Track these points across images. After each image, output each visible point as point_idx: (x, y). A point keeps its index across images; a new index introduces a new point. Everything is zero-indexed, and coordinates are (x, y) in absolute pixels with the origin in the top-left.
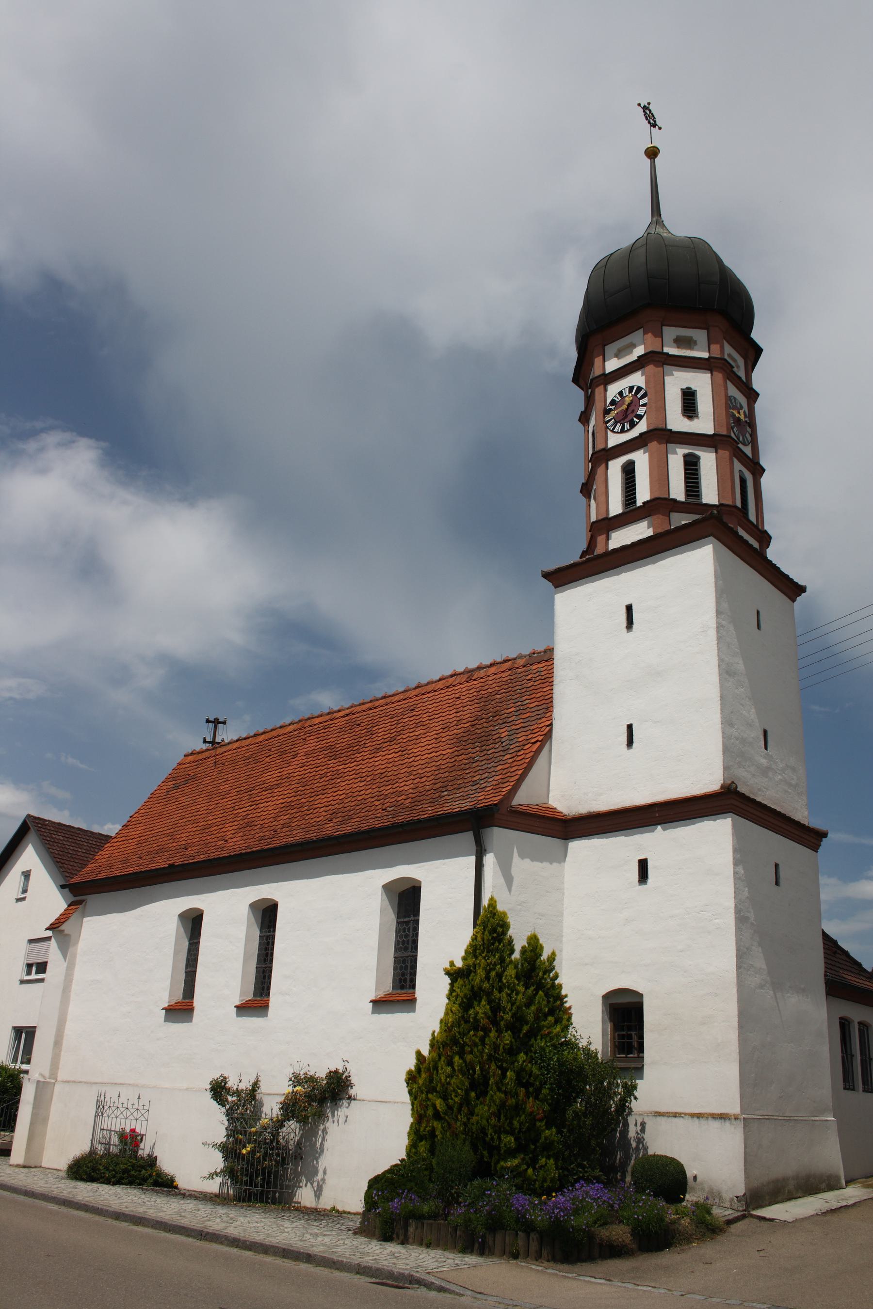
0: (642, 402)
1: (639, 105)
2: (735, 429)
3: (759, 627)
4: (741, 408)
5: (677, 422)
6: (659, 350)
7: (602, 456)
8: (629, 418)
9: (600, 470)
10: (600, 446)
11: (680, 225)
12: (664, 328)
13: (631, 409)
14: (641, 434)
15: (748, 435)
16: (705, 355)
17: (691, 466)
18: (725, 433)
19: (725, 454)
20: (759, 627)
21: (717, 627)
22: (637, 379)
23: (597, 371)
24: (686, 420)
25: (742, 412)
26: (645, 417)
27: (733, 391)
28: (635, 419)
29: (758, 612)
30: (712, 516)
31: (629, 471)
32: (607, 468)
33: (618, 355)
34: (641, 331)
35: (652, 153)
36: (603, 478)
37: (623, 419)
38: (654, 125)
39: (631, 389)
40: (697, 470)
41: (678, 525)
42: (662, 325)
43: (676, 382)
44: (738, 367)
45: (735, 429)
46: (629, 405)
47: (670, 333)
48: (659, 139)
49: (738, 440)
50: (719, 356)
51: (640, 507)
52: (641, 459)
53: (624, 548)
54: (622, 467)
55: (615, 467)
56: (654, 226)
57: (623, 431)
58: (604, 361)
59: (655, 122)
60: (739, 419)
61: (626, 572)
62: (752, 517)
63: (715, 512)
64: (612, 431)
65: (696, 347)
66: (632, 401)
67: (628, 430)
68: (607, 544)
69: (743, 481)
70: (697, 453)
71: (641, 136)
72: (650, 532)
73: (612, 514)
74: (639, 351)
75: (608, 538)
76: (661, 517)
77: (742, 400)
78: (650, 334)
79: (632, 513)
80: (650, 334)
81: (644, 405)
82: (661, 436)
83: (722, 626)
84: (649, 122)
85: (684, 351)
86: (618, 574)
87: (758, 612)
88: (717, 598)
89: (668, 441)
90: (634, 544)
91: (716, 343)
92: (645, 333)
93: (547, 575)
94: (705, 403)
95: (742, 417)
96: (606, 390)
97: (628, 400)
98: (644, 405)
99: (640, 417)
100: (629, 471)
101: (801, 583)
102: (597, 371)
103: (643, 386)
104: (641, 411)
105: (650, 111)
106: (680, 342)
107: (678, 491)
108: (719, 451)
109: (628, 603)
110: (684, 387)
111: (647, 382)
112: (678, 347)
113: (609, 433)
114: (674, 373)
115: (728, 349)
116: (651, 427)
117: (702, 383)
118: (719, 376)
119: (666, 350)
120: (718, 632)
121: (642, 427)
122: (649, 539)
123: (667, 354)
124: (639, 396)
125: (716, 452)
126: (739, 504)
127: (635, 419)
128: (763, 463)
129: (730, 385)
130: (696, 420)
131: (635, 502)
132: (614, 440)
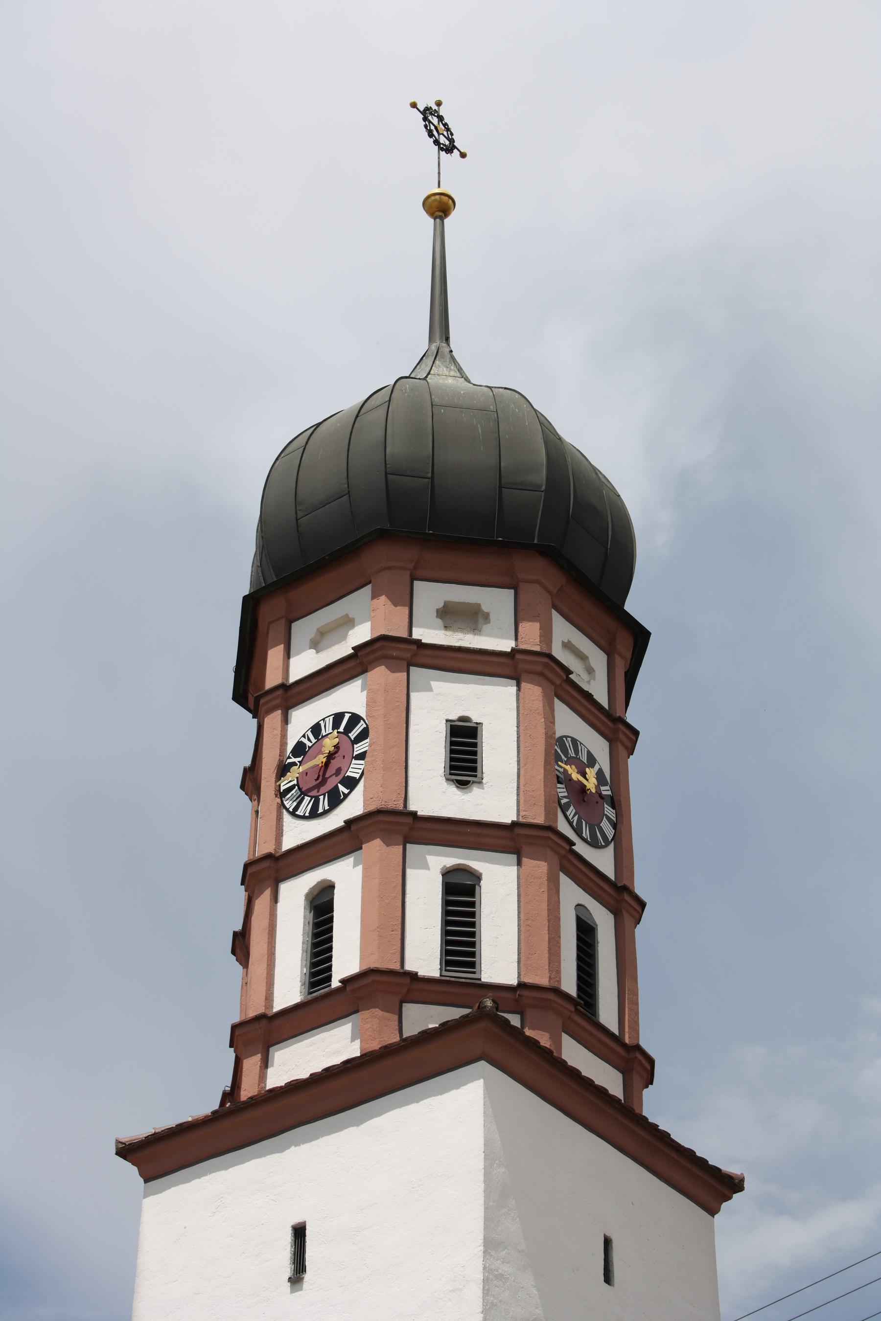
0: (359, 748)
1: (414, 105)
2: (571, 811)
3: (608, 1278)
4: (592, 761)
5: (432, 793)
6: (404, 634)
7: (265, 872)
8: (329, 786)
9: (262, 902)
10: (265, 848)
11: (487, 360)
12: (417, 584)
13: (334, 764)
14: (349, 823)
15: (606, 825)
16: (506, 645)
17: (460, 894)
18: (540, 820)
19: (539, 868)
20: (608, 1278)
21: (486, 1281)
22: (350, 697)
23: (272, 679)
24: (453, 789)
25: (591, 773)
26: (360, 787)
27: (569, 723)
28: (342, 788)
29: (607, 1242)
30: (481, 1015)
31: (321, 906)
32: (275, 899)
33: (316, 645)
34: (368, 589)
35: (440, 207)
36: (265, 923)
37: (318, 787)
38: (450, 149)
39: (338, 718)
40: (472, 904)
41: (439, 1026)
42: (413, 578)
43: (440, 701)
44: (590, 671)
45: (571, 811)
46: (331, 756)
47: (430, 595)
48: (455, 177)
49: (578, 832)
50: (537, 648)
51: (338, 990)
52: (346, 876)
53: (295, 1087)
54: (307, 895)
55: (294, 894)
56: (429, 361)
57: (314, 814)
58: (288, 655)
59: (452, 141)
60: (583, 789)
61: (297, 1144)
62: (608, 1014)
63: (489, 1003)
64: (293, 814)
65: (486, 628)
66: (337, 747)
67: (326, 812)
68: (263, 1077)
69: (586, 933)
70: (476, 865)
71: (421, 169)
72: (354, 1051)
73: (279, 1005)
74: (361, 634)
75: (266, 1063)
76: (377, 1012)
77: (596, 744)
78: (383, 598)
79: (325, 1000)
80: (383, 598)
81: (362, 756)
82: (400, 827)
83: (500, 1277)
84: (437, 142)
85: (460, 635)
86: (281, 1150)
87: (607, 1242)
88: (487, 1209)
89: (408, 840)
90: (316, 1079)
91: (531, 619)
92: (375, 596)
93: (126, 1151)
94: (499, 753)
95: (591, 784)
96: (286, 721)
97: (329, 744)
98: (362, 756)
99: (351, 784)
100: (321, 906)
101: (731, 1168)
102: (272, 679)
103: (362, 712)
104: (354, 769)
105: (441, 118)
106: (449, 615)
107: (424, 956)
108: (525, 860)
109: (296, 1220)
110: (454, 716)
111: (370, 704)
112: (446, 628)
113: (286, 817)
114: (434, 684)
115: (563, 631)
116: (372, 807)
117: (494, 707)
118: (534, 692)
119: (417, 634)
120: (486, 1292)
121: (354, 805)
122: (349, 1065)
123: (418, 643)
124: (353, 735)
125: (519, 863)
126: (569, 985)
127: (342, 788)
128: (640, 889)
129: (562, 711)
130: (475, 790)
131: (329, 979)
132: (297, 833)
